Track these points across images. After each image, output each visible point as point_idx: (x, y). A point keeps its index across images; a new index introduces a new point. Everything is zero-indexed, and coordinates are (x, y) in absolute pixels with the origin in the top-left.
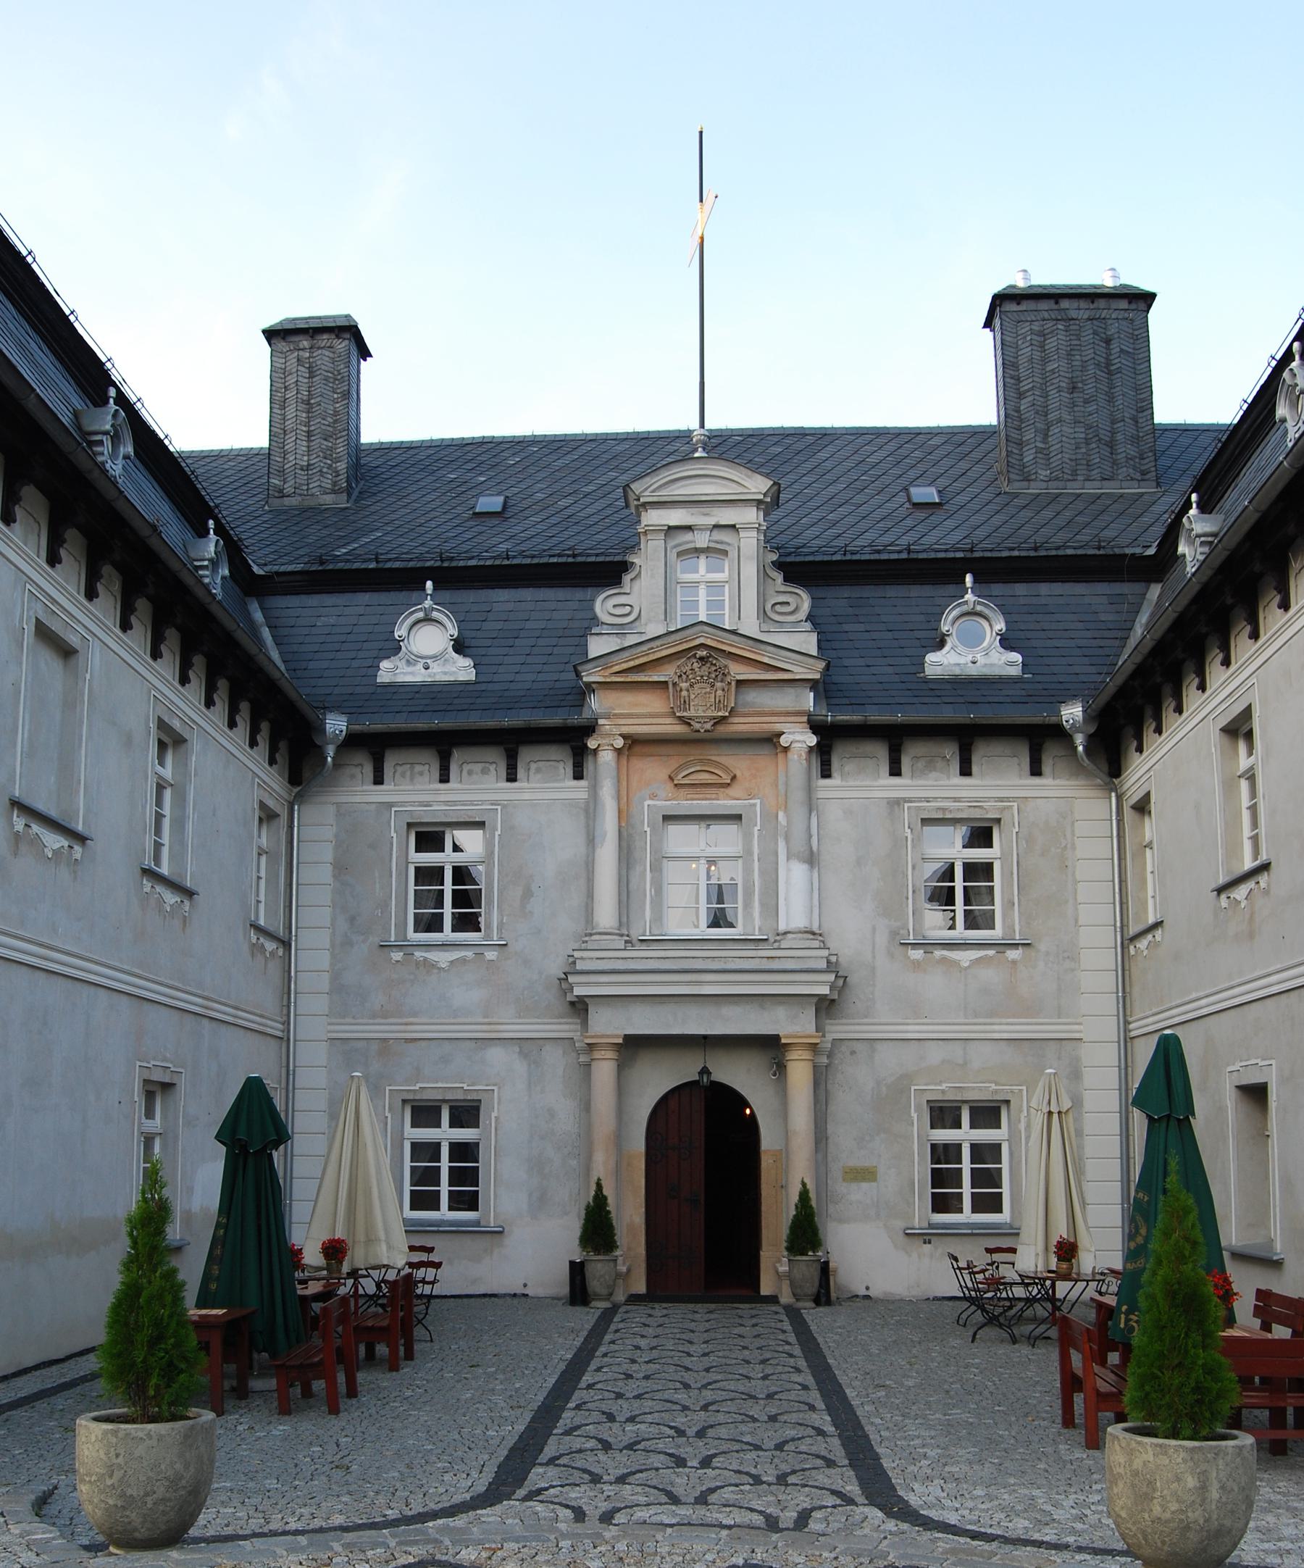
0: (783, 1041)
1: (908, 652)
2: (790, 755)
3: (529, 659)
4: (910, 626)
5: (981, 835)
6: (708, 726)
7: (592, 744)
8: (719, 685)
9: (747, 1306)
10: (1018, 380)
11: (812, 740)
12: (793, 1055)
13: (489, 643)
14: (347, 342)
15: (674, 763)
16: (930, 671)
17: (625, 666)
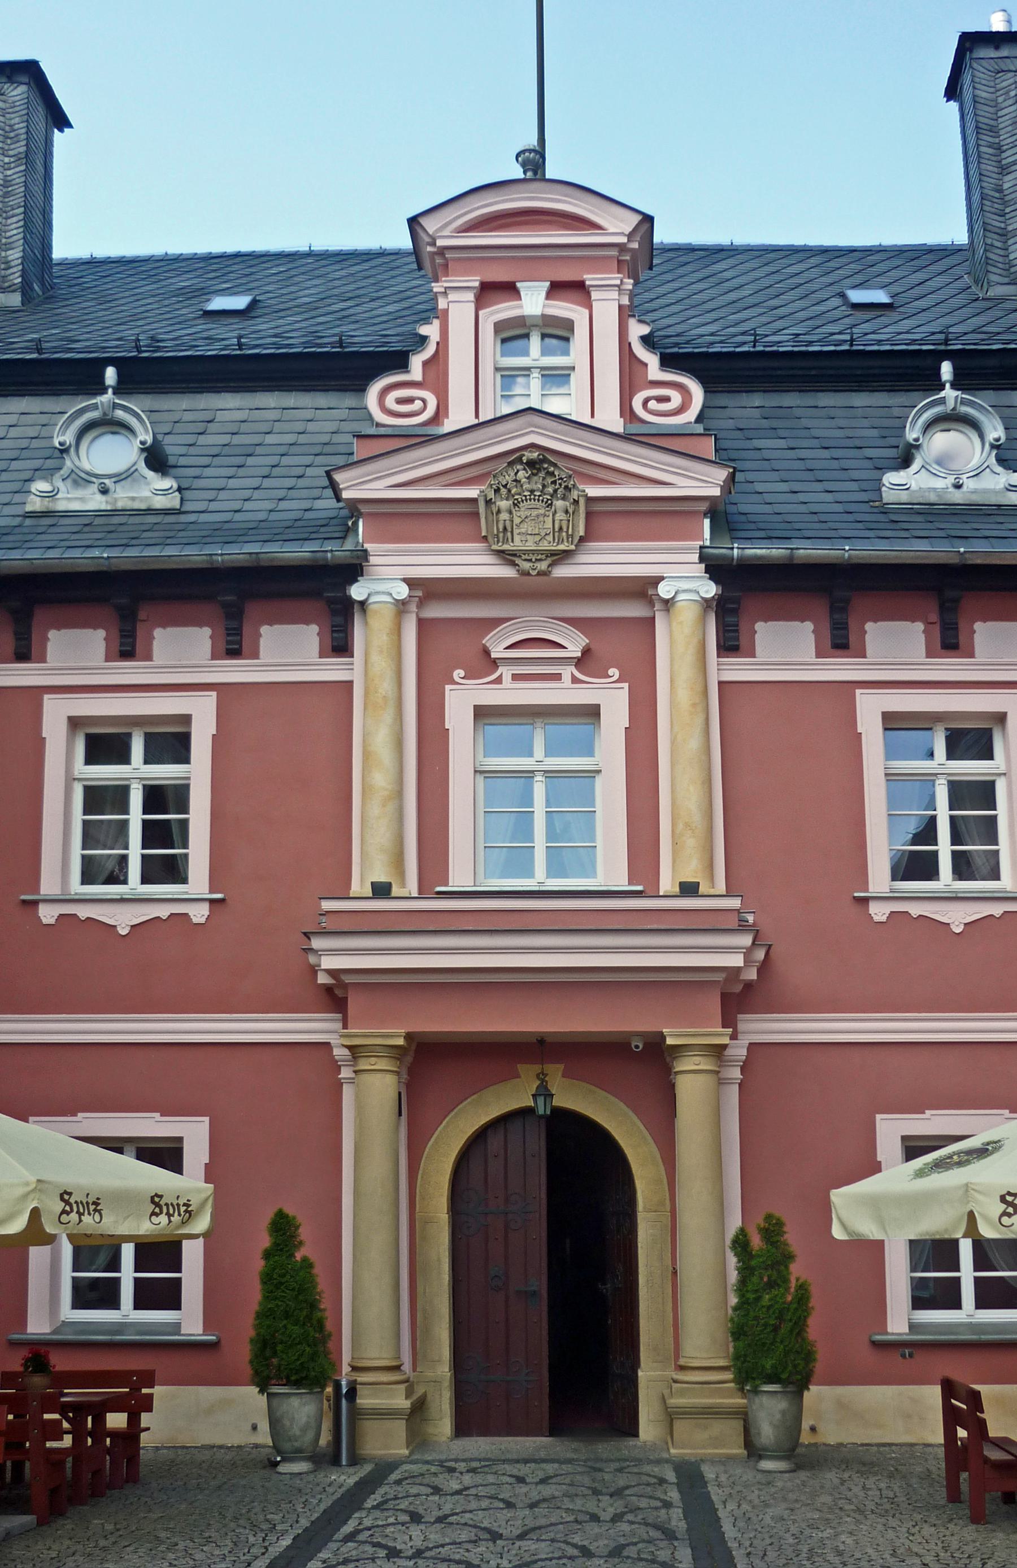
0: (669, 1041)
1: (855, 475)
3: (267, 483)
4: (858, 443)
5: (972, 739)
6: (543, 566)
7: (357, 592)
8: (559, 504)
10: (999, 148)
11: (710, 589)
12: (684, 1064)
13: (205, 461)
14: (23, 88)
16: (889, 496)
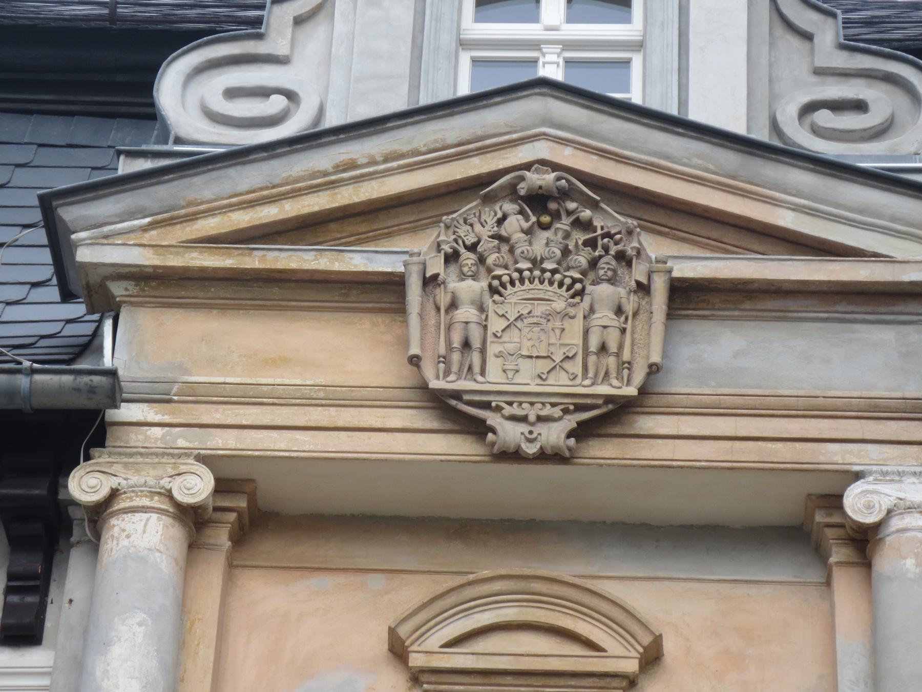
2: (886, 561)
6: (554, 435)
7: (84, 485)
9: (21, 22)
15: (412, 592)
17: (243, 219)
